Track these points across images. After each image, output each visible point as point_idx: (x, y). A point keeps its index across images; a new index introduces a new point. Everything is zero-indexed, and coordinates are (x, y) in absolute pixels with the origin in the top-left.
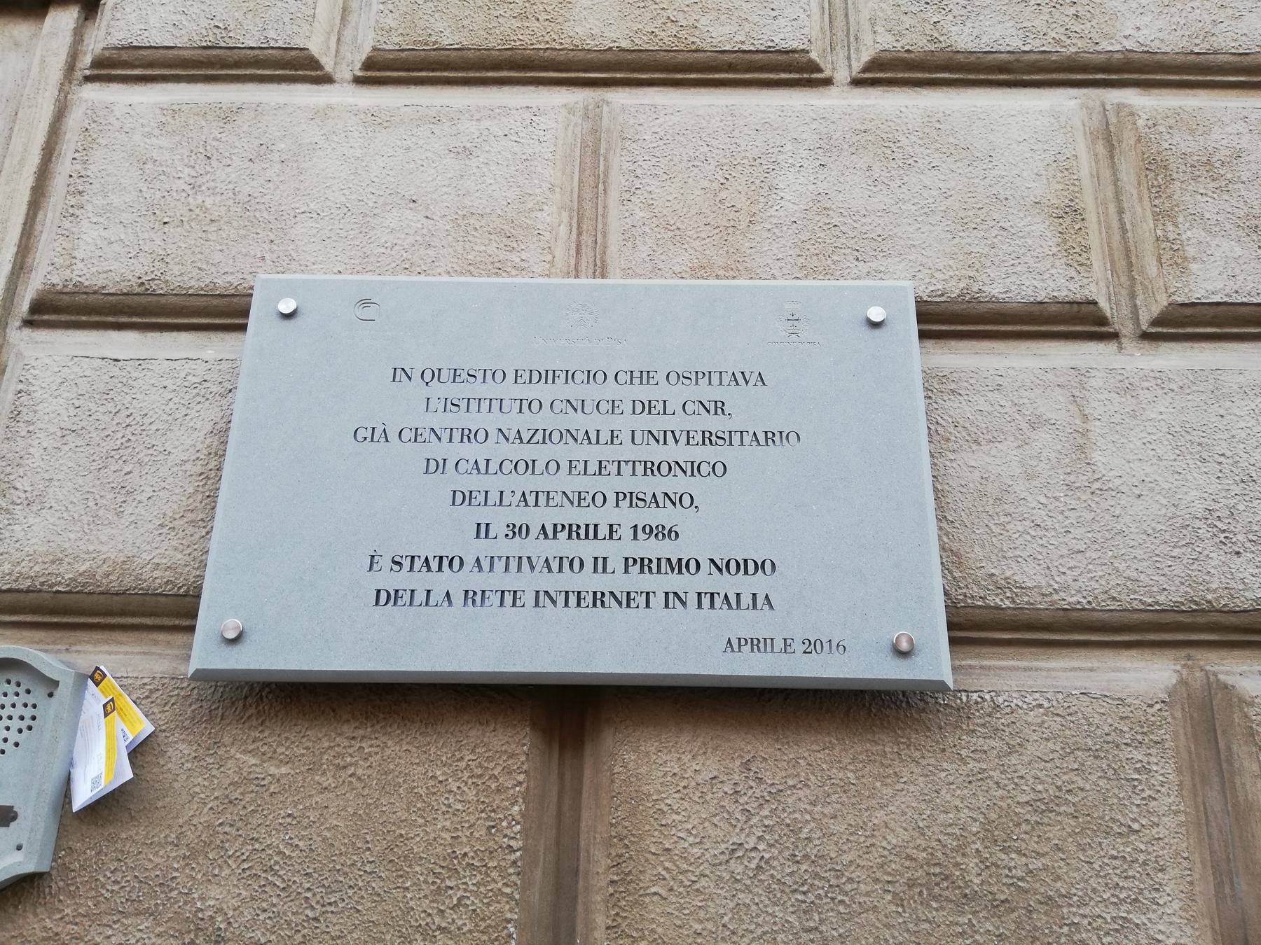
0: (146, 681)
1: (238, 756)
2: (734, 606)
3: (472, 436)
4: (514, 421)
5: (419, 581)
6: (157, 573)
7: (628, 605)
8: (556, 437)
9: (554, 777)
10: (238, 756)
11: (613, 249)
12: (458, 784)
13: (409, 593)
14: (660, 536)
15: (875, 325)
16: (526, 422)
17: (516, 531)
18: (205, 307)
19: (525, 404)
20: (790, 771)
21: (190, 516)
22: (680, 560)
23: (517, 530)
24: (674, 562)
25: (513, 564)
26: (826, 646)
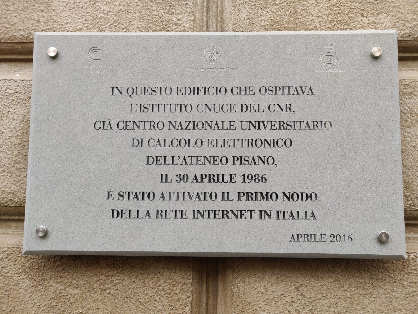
0: (5, 249)
1: (54, 285)
2: (296, 218)
3: (156, 125)
4: (178, 117)
5: (133, 205)
6: (4, 196)
7: (241, 217)
8: (200, 126)
9: (204, 291)
10: (54, 285)
11: (227, 11)
12: (159, 297)
13: (128, 211)
14: (257, 180)
15: (375, 58)
16: (183, 117)
17: (182, 178)
18: (12, 50)
19: (183, 107)
20: (318, 292)
21: (18, 166)
22: (267, 193)
23: (182, 178)
24: (264, 194)
25: (181, 196)
26: (342, 238)
